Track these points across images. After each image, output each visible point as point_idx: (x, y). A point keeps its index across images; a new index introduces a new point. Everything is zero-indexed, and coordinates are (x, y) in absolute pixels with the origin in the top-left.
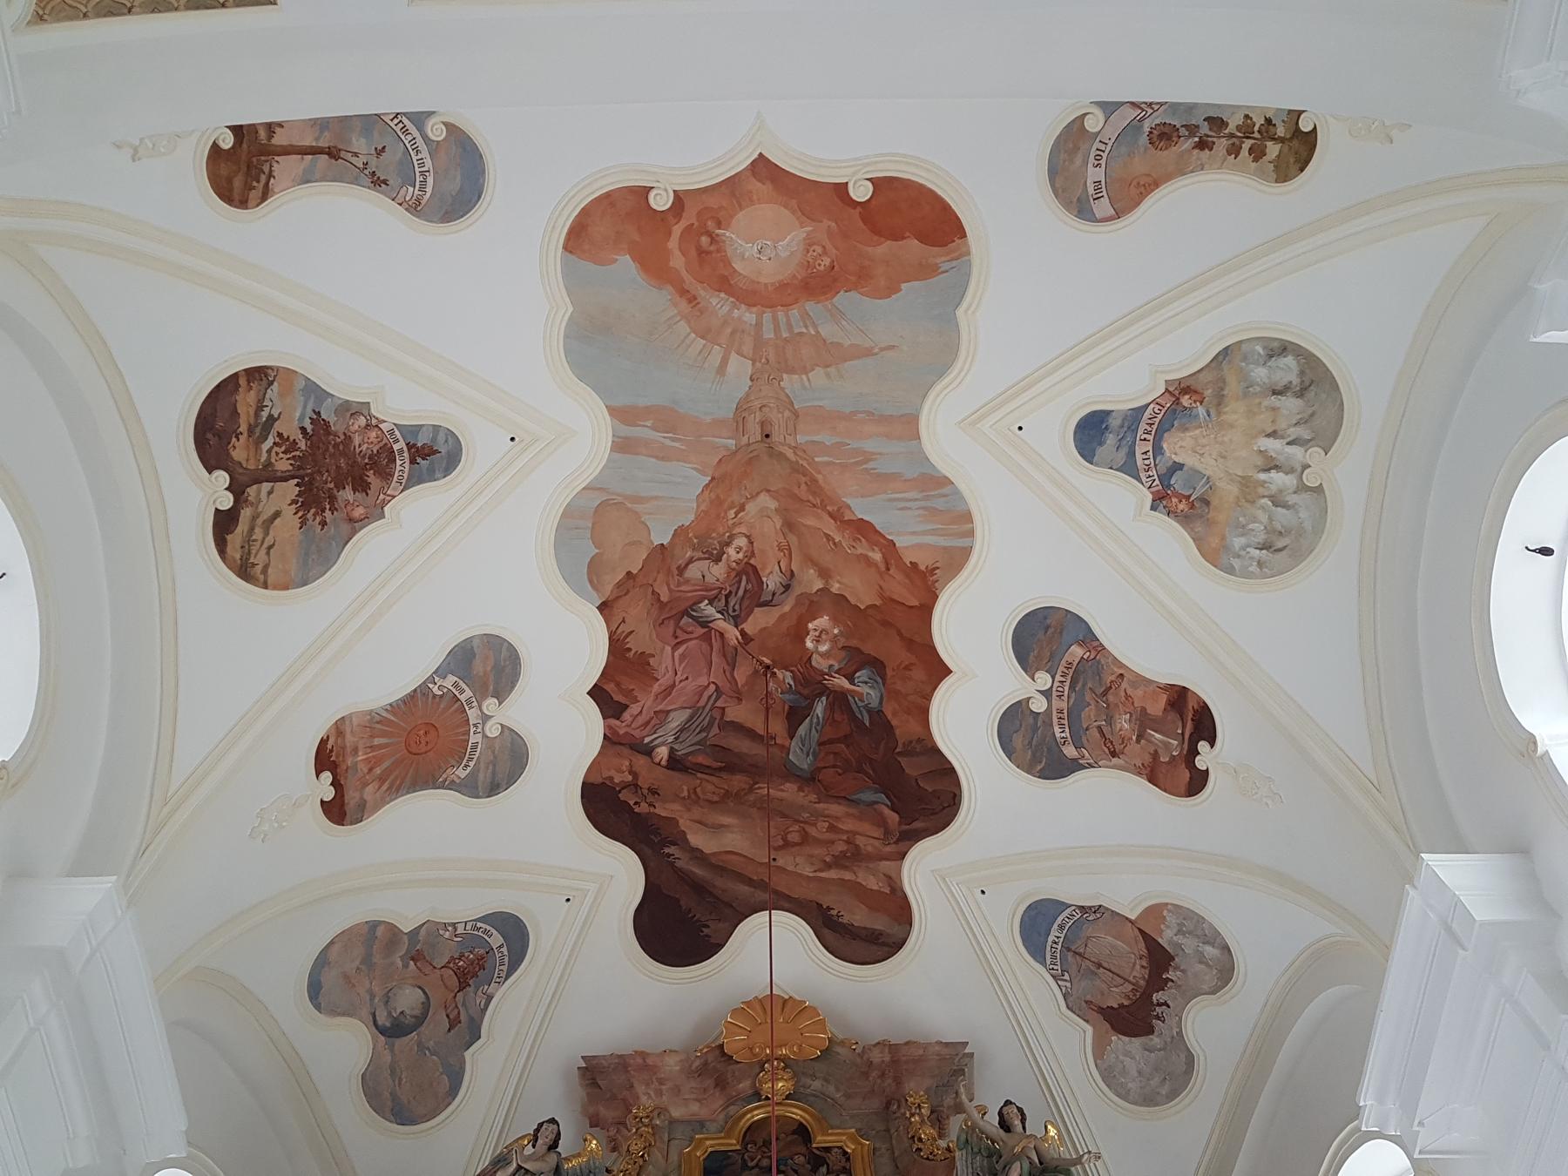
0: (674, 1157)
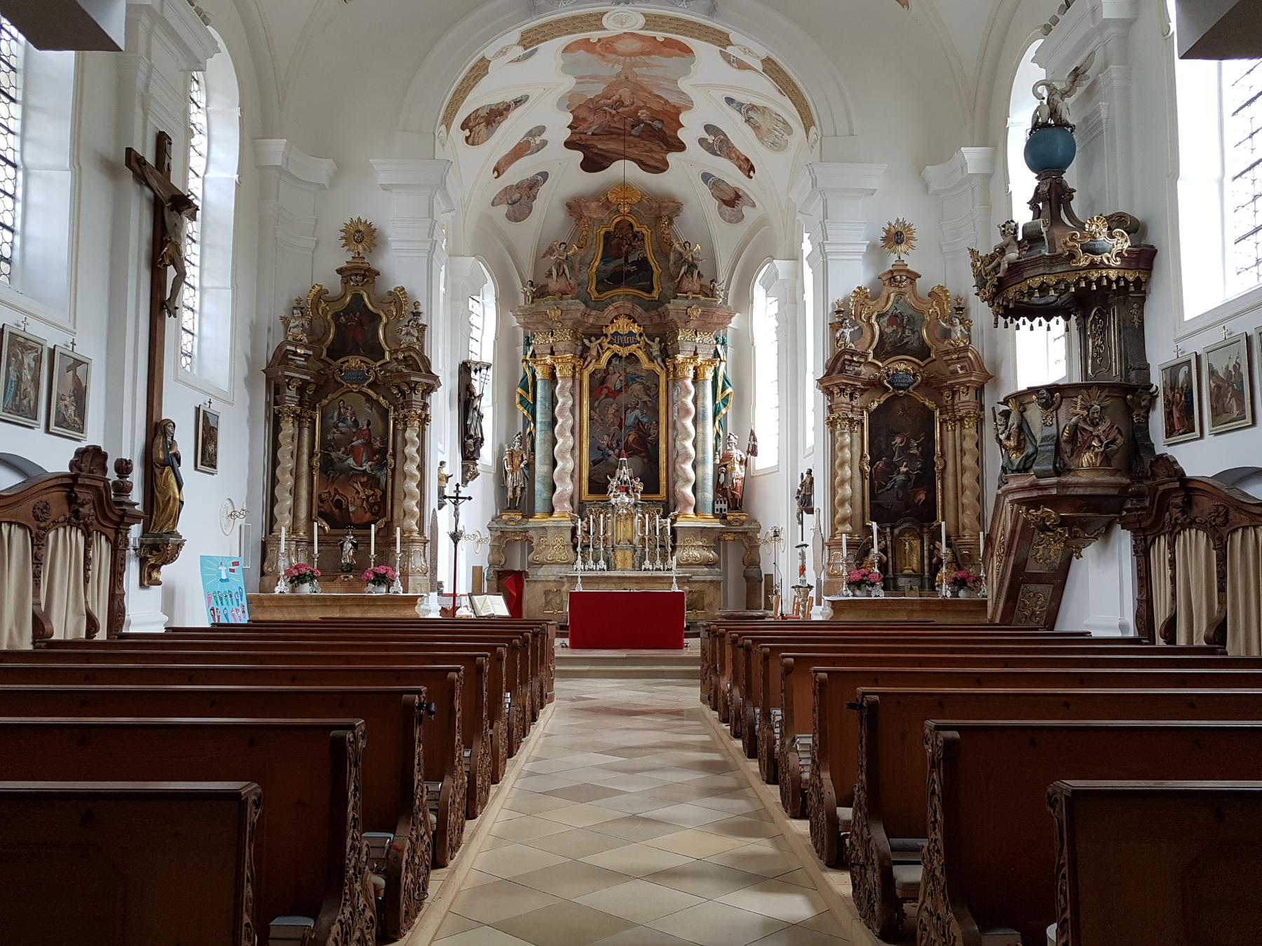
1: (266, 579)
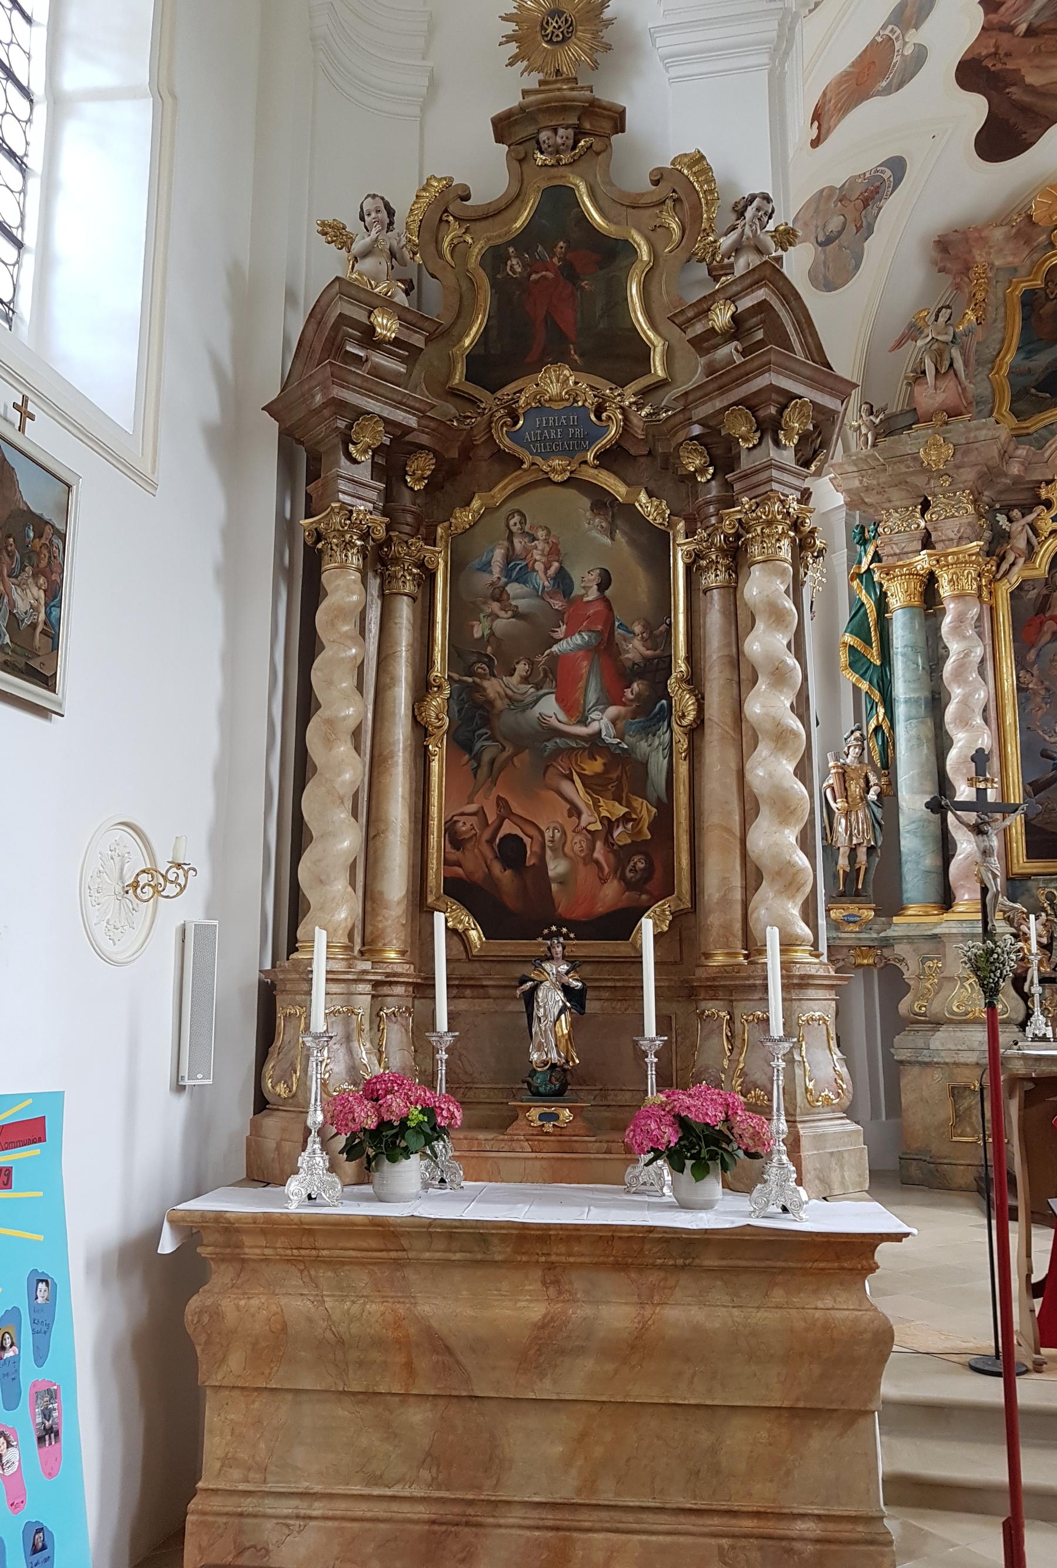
0: (1000, 295)
1: (271, 1123)
